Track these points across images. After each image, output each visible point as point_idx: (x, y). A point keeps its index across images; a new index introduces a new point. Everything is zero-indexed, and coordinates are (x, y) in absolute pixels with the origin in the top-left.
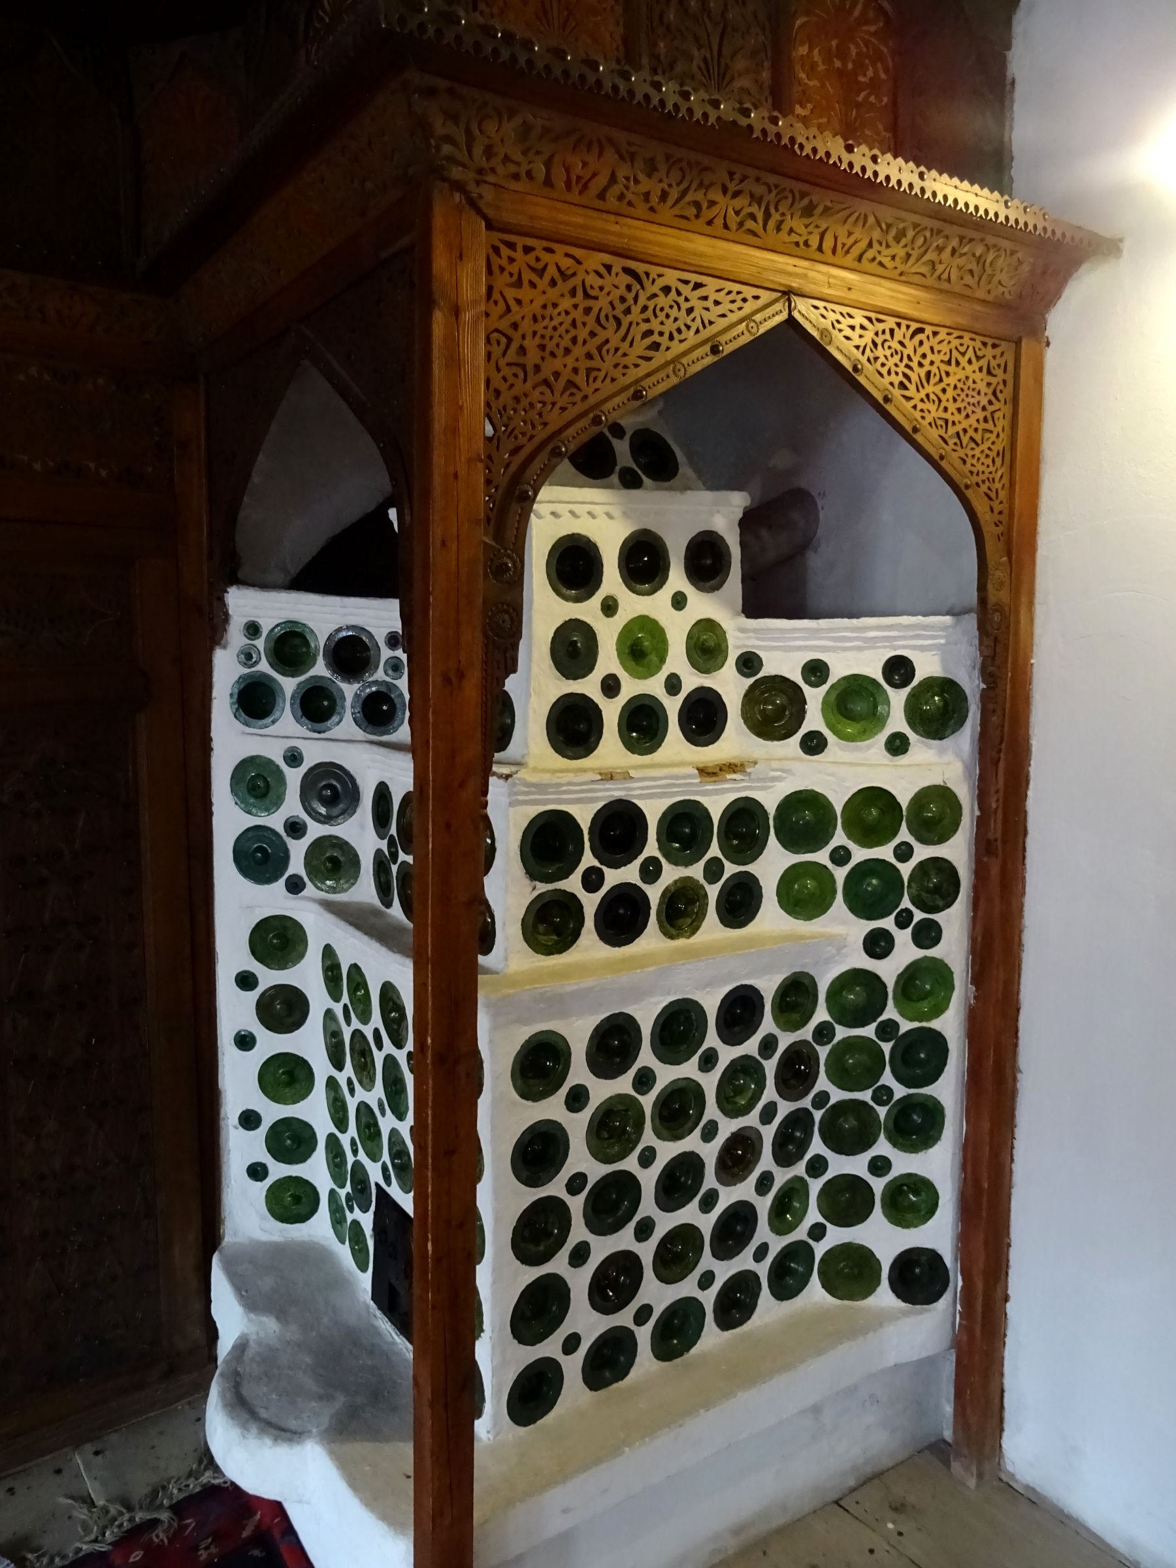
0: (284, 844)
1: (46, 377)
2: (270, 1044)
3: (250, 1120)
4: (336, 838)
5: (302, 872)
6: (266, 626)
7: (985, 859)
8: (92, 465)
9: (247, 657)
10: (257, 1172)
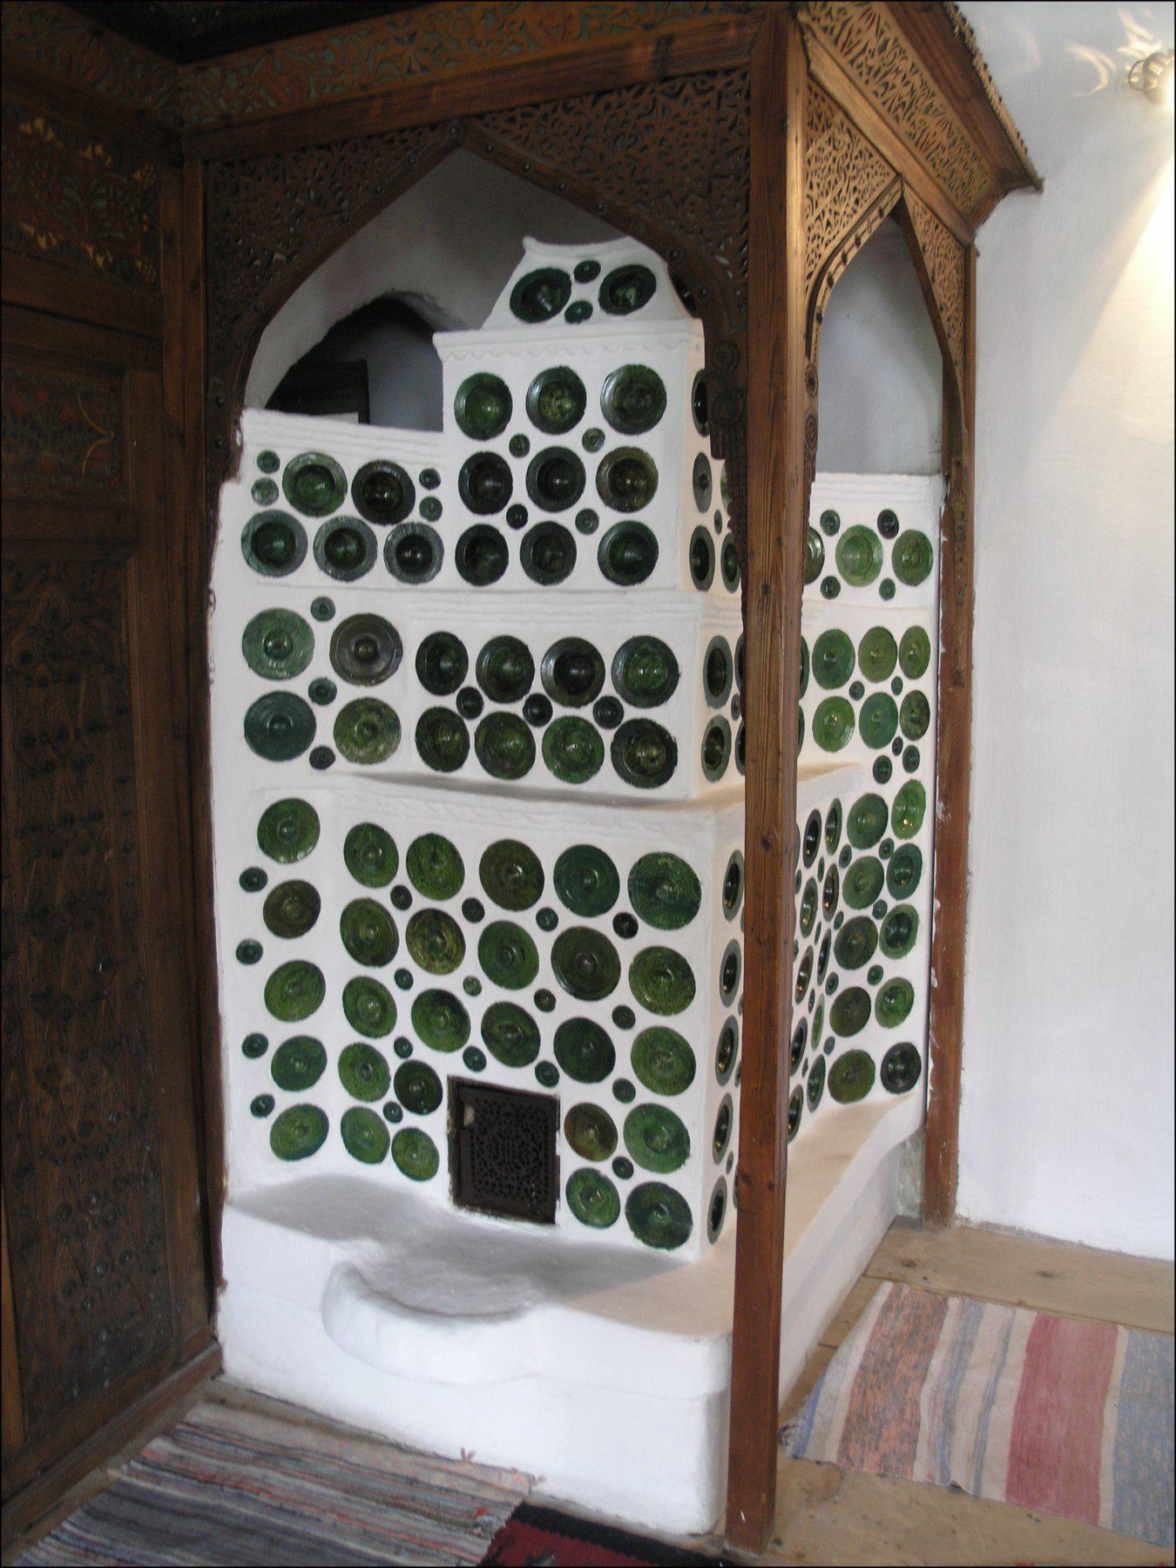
0: (310, 712)
1: (51, 135)
2: (279, 951)
3: (254, 1046)
4: (373, 700)
5: (331, 743)
6: (285, 458)
7: (951, 690)
8: (90, 250)
9: (264, 490)
10: (261, 1106)
